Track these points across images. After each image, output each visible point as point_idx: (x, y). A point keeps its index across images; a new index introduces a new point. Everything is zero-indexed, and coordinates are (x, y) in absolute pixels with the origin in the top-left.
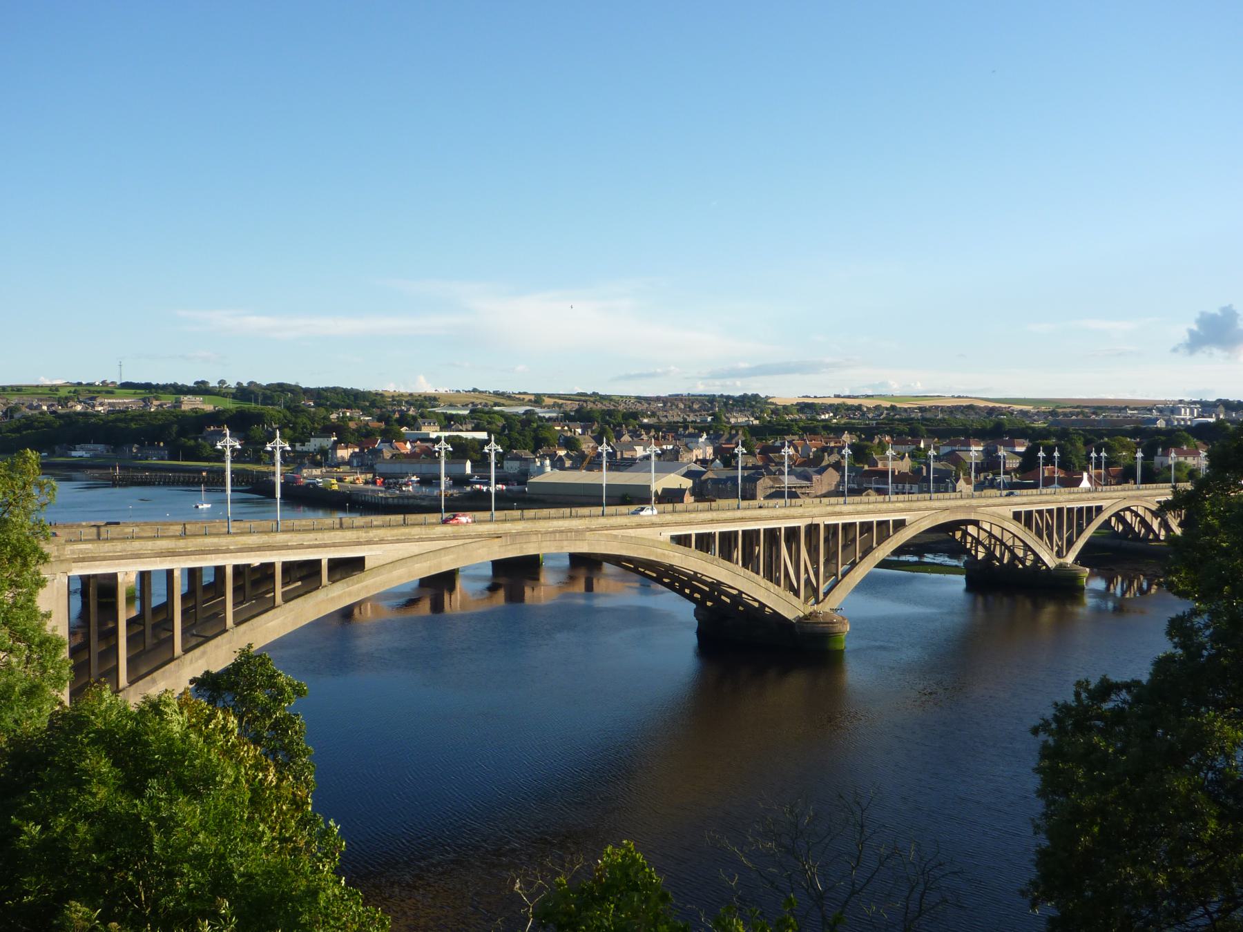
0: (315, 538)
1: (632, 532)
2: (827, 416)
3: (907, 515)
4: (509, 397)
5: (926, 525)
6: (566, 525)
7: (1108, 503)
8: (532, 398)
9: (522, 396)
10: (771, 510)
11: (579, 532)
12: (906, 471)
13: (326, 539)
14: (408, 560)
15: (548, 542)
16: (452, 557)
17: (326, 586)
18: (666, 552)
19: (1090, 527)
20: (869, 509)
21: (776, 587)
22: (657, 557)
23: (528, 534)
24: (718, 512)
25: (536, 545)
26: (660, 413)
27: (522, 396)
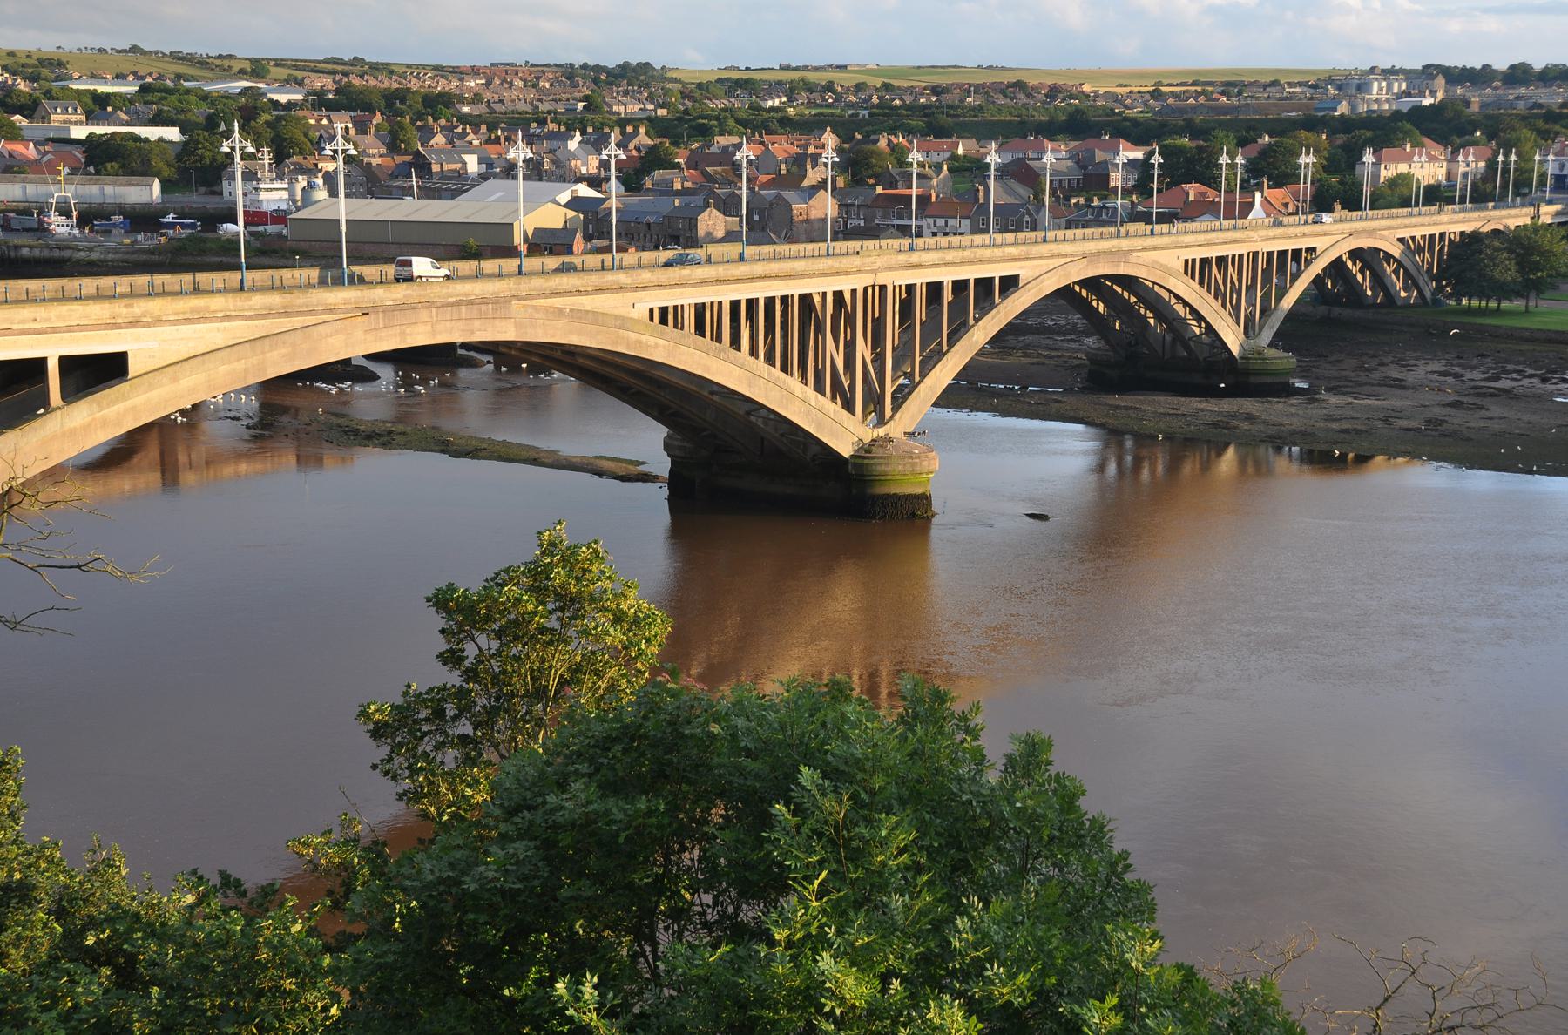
0: (32, 317)
1: (587, 302)
2: (777, 102)
3: (1021, 268)
4: (203, 63)
5: (1051, 285)
6: (477, 291)
7: (1328, 241)
8: (247, 66)
9: (226, 63)
10: (810, 261)
11: (499, 302)
12: (715, 211)
13: (54, 318)
14: (207, 356)
15: (448, 323)
16: (284, 351)
17: (59, 408)
18: (644, 338)
19: (1297, 283)
20: (963, 258)
21: (819, 395)
22: (628, 348)
23: (414, 308)
24: (727, 266)
25: (429, 327)
26: (487, 95)
27: (226, 63)
